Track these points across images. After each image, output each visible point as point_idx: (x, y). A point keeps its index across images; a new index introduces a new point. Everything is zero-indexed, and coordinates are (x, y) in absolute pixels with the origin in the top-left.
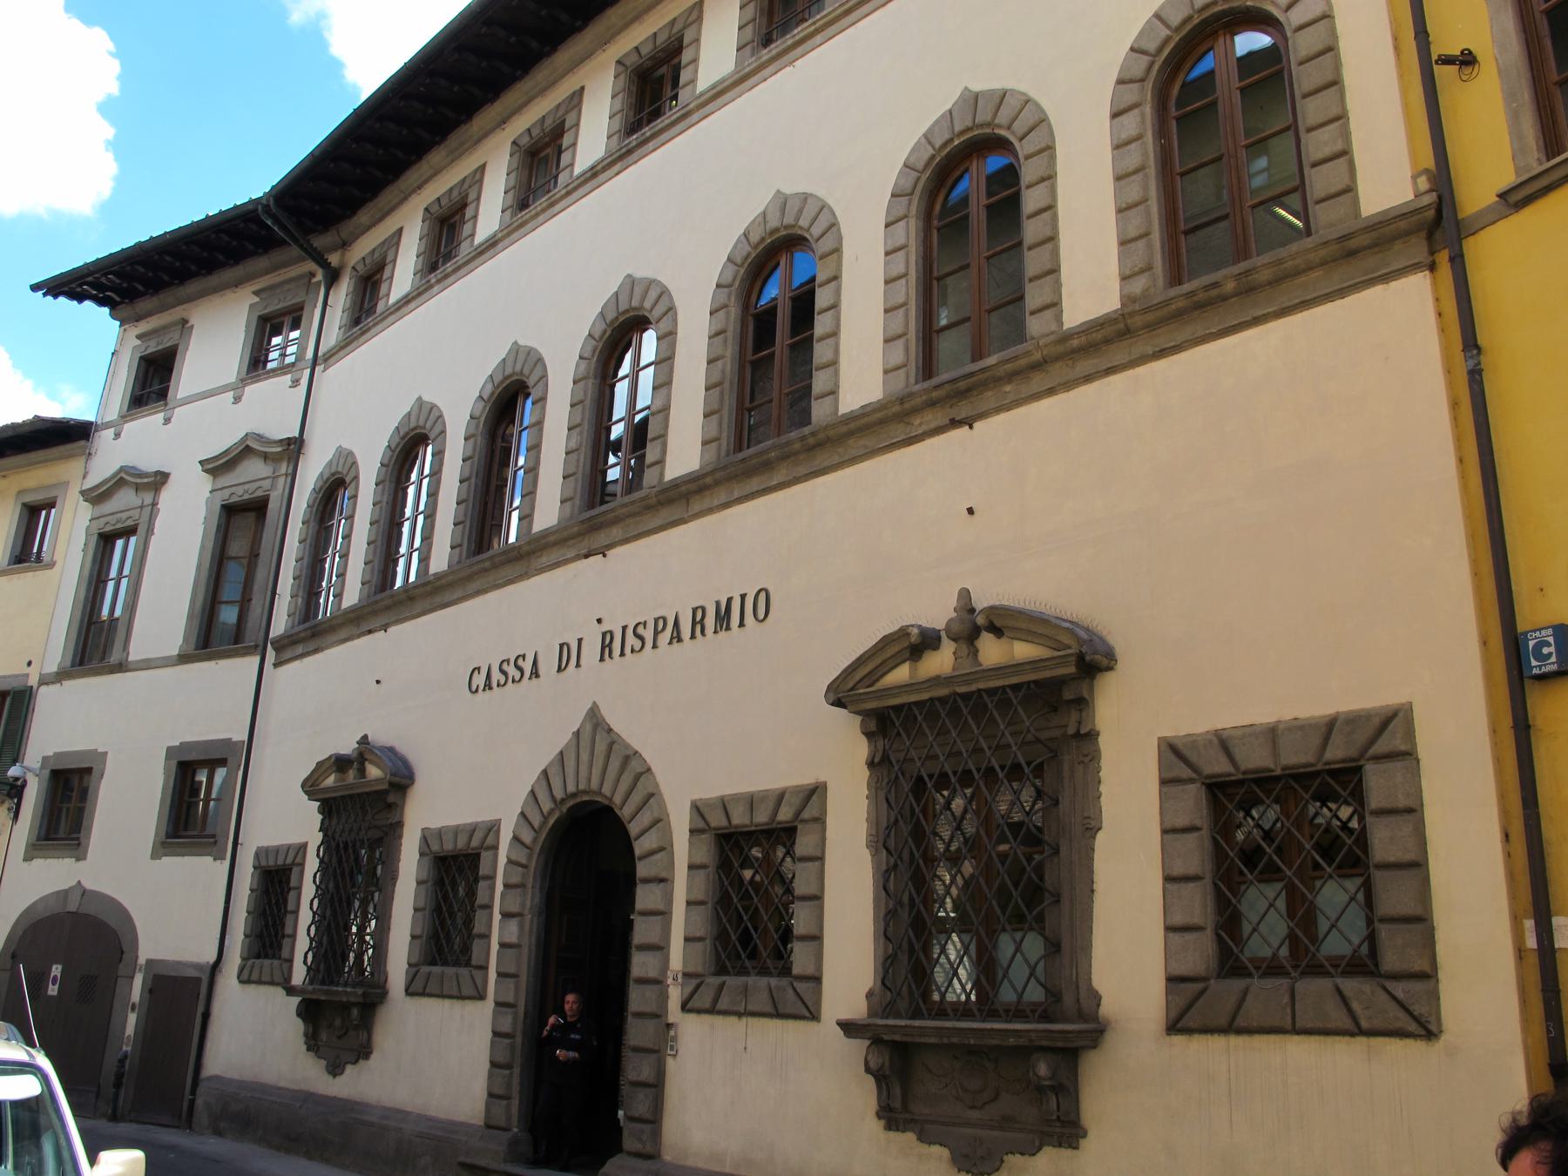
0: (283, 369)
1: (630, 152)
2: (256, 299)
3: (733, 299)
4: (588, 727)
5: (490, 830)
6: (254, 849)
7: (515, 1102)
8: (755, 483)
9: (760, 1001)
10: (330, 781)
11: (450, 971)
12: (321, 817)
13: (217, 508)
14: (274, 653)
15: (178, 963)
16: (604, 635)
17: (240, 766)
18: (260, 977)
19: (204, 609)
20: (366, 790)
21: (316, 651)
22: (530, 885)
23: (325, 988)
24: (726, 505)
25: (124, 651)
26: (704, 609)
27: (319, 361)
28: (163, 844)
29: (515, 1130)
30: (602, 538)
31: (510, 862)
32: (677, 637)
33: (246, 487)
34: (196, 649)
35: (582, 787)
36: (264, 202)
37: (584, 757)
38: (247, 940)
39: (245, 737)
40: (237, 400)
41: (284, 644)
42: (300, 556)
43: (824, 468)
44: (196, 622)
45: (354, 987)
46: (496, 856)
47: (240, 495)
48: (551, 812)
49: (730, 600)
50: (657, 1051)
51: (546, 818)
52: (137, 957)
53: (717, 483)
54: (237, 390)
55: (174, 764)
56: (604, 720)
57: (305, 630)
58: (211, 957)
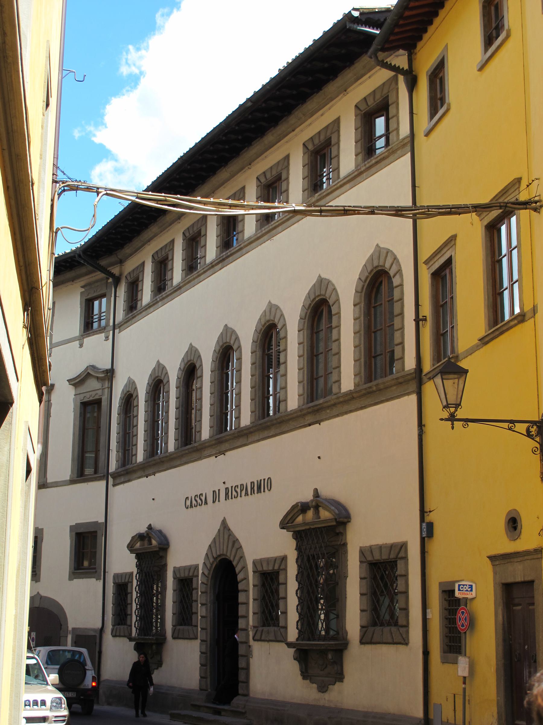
0: (101, 330)
1: (224, 260)
2: (83, 290)
3: (258, 348)
4: (222, 528)
5: (195, 569)
6: (112, 575)
7: (209, 680)
8: (266, 433)
9: (272, 637)
10: (138, 545)
11: (186, 628)
12: (136, 560)
13: (79, 404)
14: (112, 479)
15: (86, 629)
16: (226, 489)
17: (103, 534)
18: (178, 636)
19: (78, 456)
20: (151, 550)
21: (129, 481)
22: (209, 592)
23: (142, 637)
24: (258, 441)
25: (44, 477)
26: (254, 482)
27: (116, 327)
28: (73, 573)
29: (209, 690)
30: (223, 447)
31: (202, 583)
32: (247, 494)
33: (91, 393)
34: (77, 477)
35: (221, 553)
36: (78, 252)
37: (222, 540)
38: (114, 617)
39: (103, 520)
40: (81, 346)
41: (115, 476)
42: (118, 432)
43: (284, 432)
44: (76, 463)
45: (153, 636)
46: (198, 579)
47: (88, 397)
48: (213, 562)
49: (261, 480)
50: (246, 656)
51: (212, 565)
52: (68, 627)
53: (255, 431)
54: (81, 338)
55: (74, 534)
56: (227, 525)
57: (123, 471)
58: (99, 625)
